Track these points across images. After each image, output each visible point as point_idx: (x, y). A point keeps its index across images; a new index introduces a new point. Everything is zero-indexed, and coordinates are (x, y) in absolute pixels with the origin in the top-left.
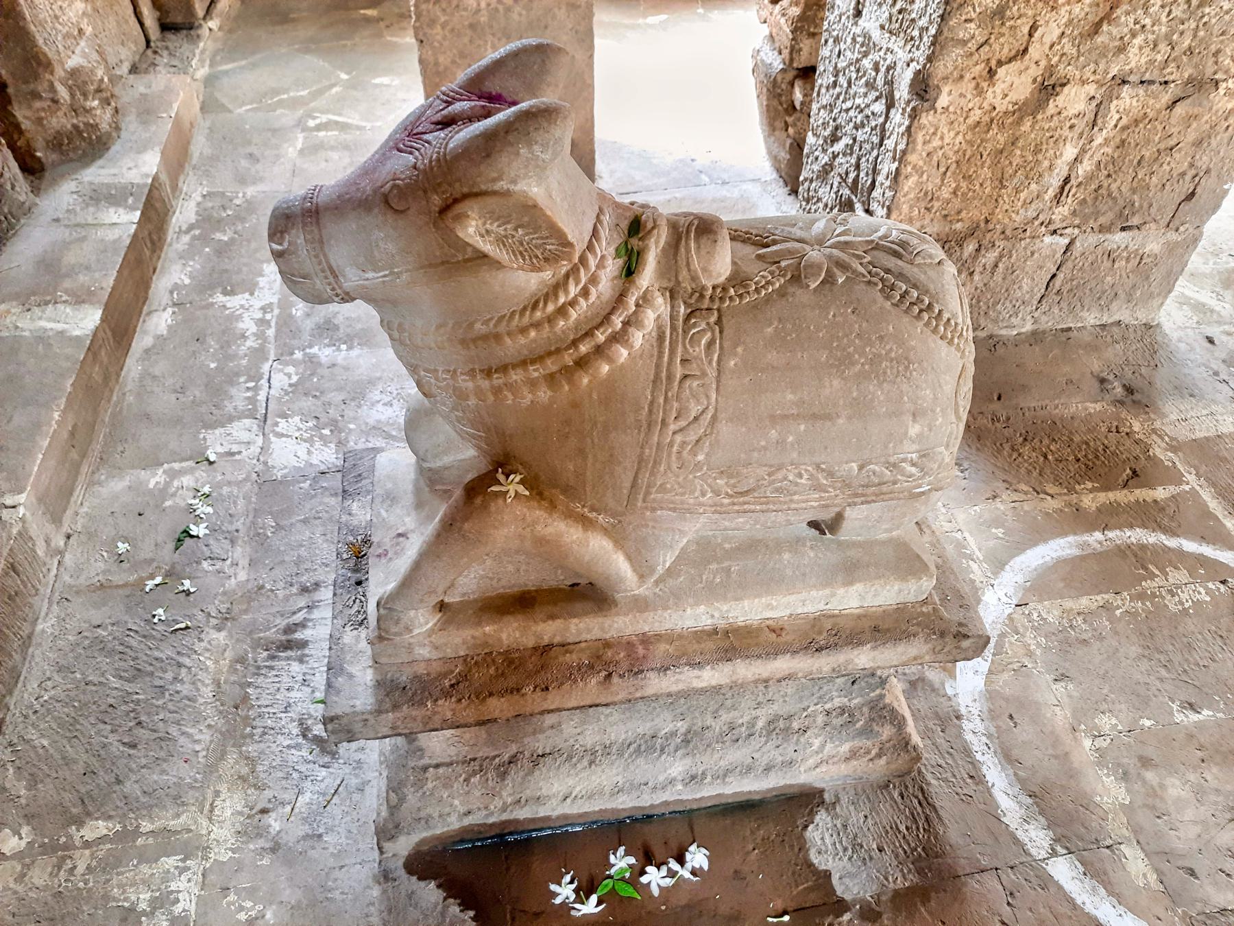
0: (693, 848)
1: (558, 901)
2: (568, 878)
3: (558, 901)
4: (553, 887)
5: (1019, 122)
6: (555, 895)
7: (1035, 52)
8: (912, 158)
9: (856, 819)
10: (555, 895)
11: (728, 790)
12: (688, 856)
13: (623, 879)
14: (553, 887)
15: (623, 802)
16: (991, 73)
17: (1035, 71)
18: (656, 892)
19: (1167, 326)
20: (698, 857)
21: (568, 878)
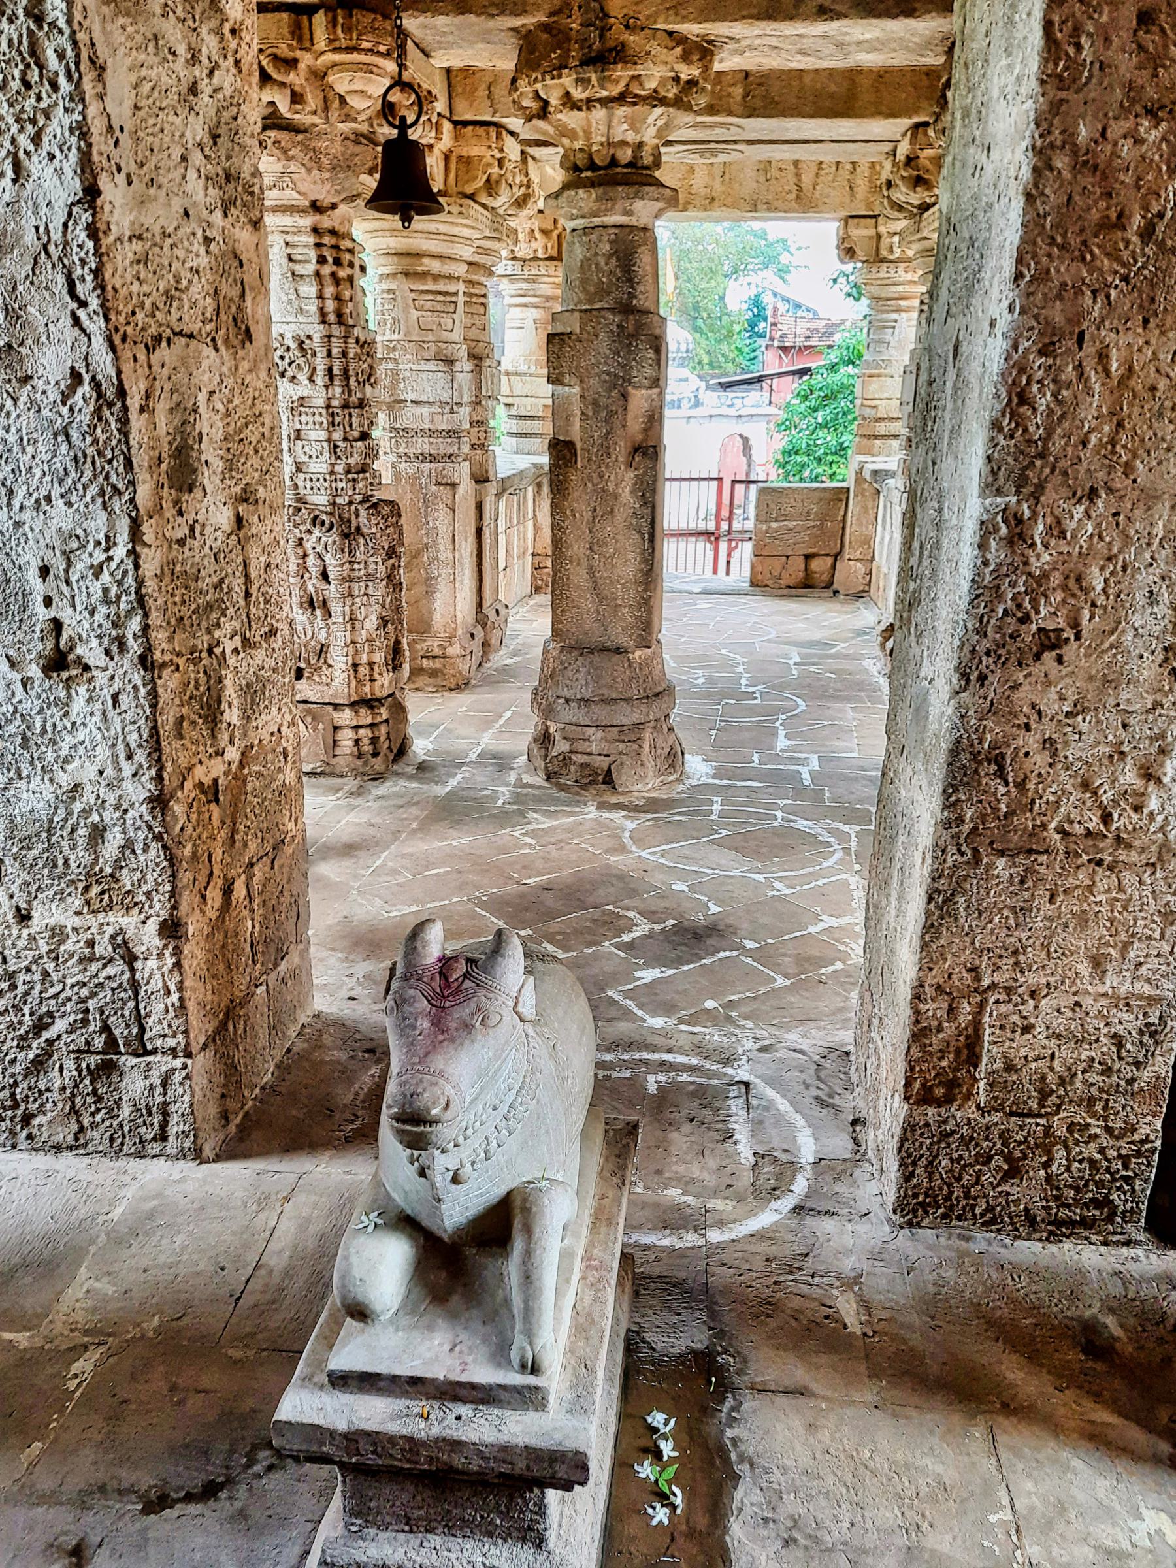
0: (649, 1420)
1: (666, 1522)
2: (650, 1511)
3: (666, 1522)
4: (654, 1522)
5: (223, 922)
6: (661, 1522)
7: (216, 872)
8: (187, 983)
9: (655, 1319)
10: (661, 1522)
11: (911, 928)
12: (655, 1424)
13: (660, 1473)
14: (654, 1522)
15: (830, 1080)
16: (204, 897)
17: (220, 882)
18: (676, 1454)
19: (325, 1009)
20: (657, 1419)
21: (650, 1511)
